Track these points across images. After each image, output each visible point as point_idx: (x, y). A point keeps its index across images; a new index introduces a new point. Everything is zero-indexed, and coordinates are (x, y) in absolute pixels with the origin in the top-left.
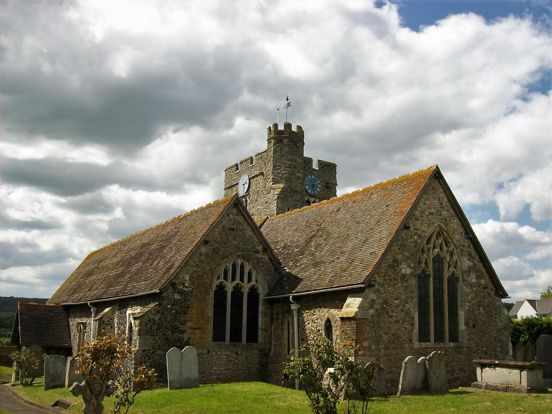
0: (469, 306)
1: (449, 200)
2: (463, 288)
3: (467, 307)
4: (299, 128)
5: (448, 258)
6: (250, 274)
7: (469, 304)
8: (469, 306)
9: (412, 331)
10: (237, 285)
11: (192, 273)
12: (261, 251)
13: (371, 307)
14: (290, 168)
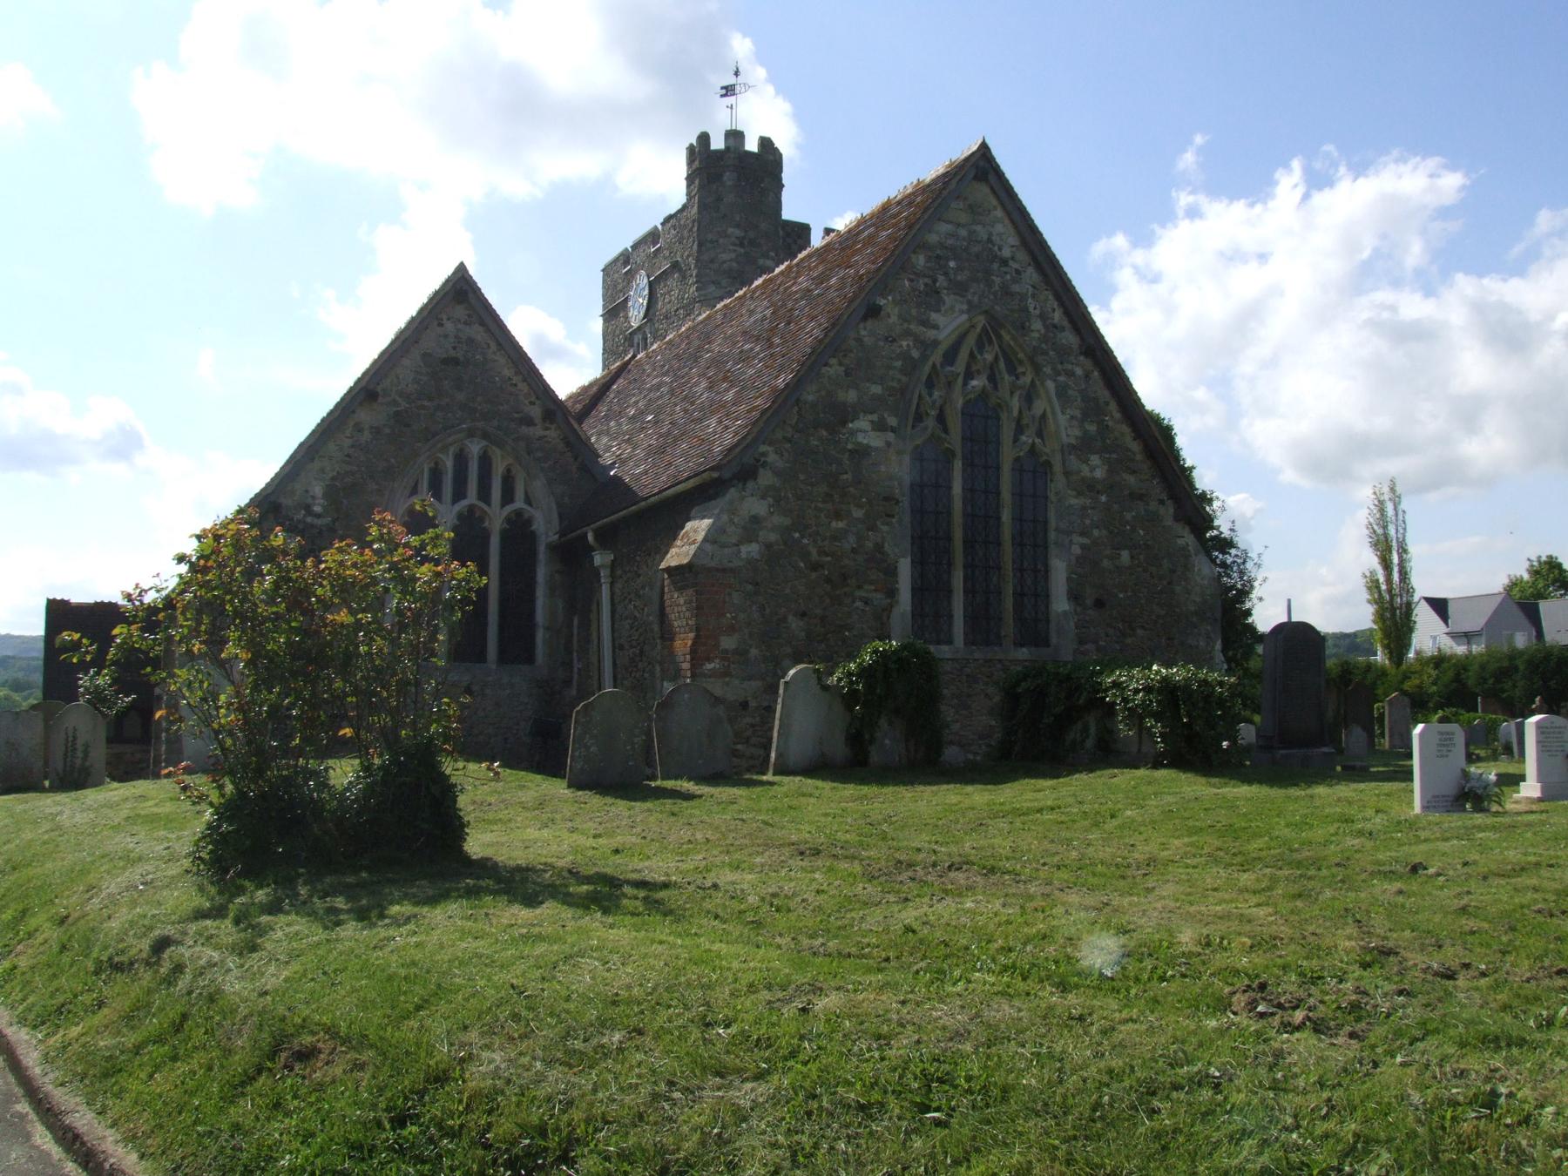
0: (1083, 547)
1: (1024, 243)
2: (1063, 498)
3: (1076, 550)
4: (766, 143)
5: (1015, 403)
6: (508, 481)
7: (1085, 541)
8: (1083, 547)
9: (889, 609)
10: (471, 508)
11: (333, 479)
12: (538, 421)
13: (749, 535)
14: (741, 245)
